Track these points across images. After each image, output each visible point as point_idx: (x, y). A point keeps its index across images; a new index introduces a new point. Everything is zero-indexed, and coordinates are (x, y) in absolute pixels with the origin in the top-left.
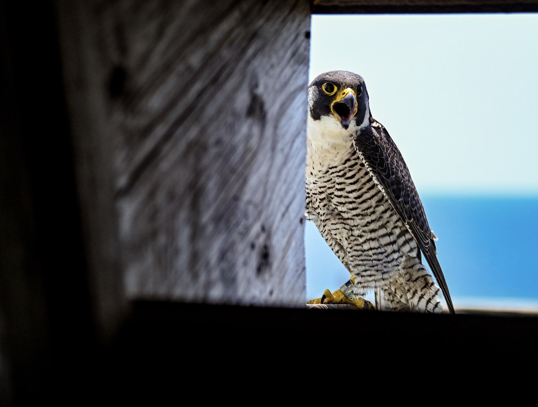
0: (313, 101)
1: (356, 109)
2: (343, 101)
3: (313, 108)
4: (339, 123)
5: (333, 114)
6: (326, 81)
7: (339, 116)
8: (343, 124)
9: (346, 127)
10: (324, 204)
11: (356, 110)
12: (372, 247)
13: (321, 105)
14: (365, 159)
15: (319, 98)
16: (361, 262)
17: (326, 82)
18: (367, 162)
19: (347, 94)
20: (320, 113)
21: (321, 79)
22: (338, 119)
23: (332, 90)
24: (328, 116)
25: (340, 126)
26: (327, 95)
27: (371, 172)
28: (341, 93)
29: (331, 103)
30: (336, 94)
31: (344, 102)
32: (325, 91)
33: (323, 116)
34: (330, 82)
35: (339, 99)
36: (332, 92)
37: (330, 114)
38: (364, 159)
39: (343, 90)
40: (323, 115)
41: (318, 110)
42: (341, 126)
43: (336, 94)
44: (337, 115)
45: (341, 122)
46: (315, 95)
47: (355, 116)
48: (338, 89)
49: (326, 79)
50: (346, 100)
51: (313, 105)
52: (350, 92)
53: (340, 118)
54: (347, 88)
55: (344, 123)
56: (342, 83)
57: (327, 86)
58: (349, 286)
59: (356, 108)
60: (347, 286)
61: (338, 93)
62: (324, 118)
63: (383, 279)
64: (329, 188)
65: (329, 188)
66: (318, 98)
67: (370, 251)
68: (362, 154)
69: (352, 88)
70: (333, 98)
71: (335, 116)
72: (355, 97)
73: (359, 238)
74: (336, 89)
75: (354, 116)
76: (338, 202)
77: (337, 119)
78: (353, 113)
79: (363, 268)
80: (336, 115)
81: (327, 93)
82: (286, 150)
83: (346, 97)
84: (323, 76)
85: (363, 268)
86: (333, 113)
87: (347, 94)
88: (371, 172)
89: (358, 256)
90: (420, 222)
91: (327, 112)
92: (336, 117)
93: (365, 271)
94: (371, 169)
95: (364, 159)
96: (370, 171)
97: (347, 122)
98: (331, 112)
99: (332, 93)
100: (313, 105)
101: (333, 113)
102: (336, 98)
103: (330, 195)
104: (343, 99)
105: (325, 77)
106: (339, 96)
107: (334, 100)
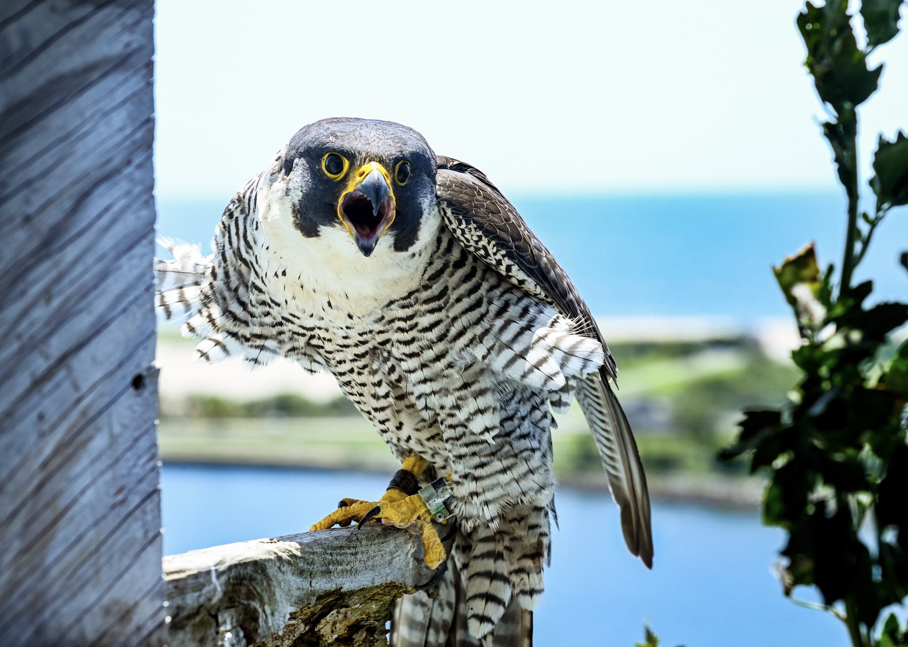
0: (302, 192)
1: (392, 213)
2: (359, 190)
3: (300, 206)
4: (352, 240)
5: (341, 224)
6: (328, 150)
7: (353, 228)
8: (360, 243)
9: (367, 251)
10: (363, 365)
11: (392, 216)
12: (489, 426)
13: (317, 203)
14: (486, 237)
15: (314, 186)
16: (464, 450)
17: (328, 152)
18: (492, 239)
19: (367, 175)
20: (315, 219)
21: (318, 145)
22: (351, 233)
23: (340, 168)
24: (333, 227)
25: (355, 247)
26: (329, 181)
27: (506, 259)
28: (357, 173)
29: (338, 197)
30: (347, 175)
31: (361, 191)
32: (326, 172)
33: (321, 226)
34: (334, 150)
35: (351, 187)
36: (341, 172)
37: (336, 222)
38: (483, 237)
39: (360, 166)
40: (323, 225)
41: (311, 214)
42: (357, 248)
43: (347, 175)
44: (350, 224)
45: (357, 240)
46: (307, 179)
47: (392, 228)
48: (352, 165)
49: (327, 145)
50: (365, 188)
51: (299, 201)
52: (375, 172)
53: (354, 231)
54: (370, 161)
55: (365, 242)
56: (359, 153)
57: (329, 162)
58: (440, 490)
59: (393, 210)
60: (435, 489)
61: (351, 174)
62: (325, 230)
63: (531, 471)
64: (380, 332)
65: (380, 332)
66: (312, 188)
67: (486, 434)
68: (475, 229)
69: (381, 161)
70: (340, 186)
71: (346, 228)
72: (387, 182)
73: (456, 412)
74: (346, 164)
75: (389, 228)
76: (404, 354)
77: (349, 233)
78: (386, 223)
79: (476, 460)
80: (348, 224)
81: (329, 175)
82: (52, 216)
83: (363, 183)
84: (323, 137)
85: (476, 460)
86: (341, 219)
87: (367, 175)
88: (506, 259)
89: (457, 439)
90: (598, 445)
91: (330, 218)
92: (348, 228)
93: (482, 465)
94: (503, 252)
95: (483, 237)
96: (504, 256)
97: (372, 241)
98: (338, 218)
99: (339, 175)
100: (299, 201)
101: (341, 219)
102: (347, 185)
103: (383, 345)
104: (359, 186)
105: (327, 140)
106: (353, 180)
107: (343, 189)
